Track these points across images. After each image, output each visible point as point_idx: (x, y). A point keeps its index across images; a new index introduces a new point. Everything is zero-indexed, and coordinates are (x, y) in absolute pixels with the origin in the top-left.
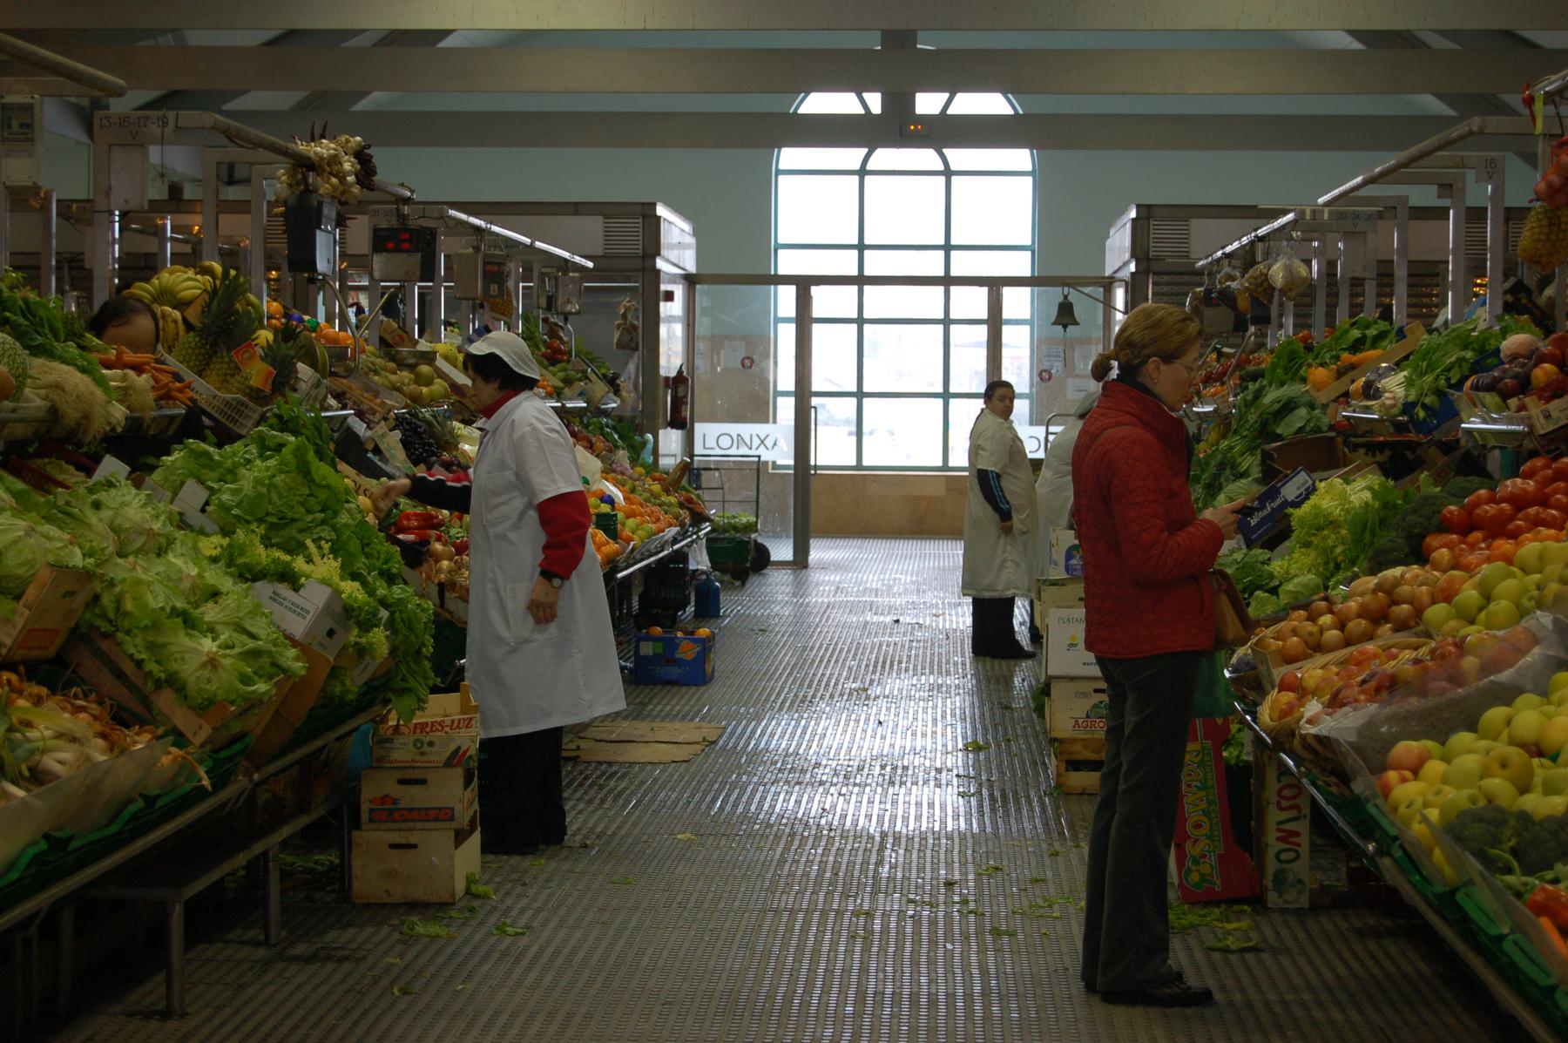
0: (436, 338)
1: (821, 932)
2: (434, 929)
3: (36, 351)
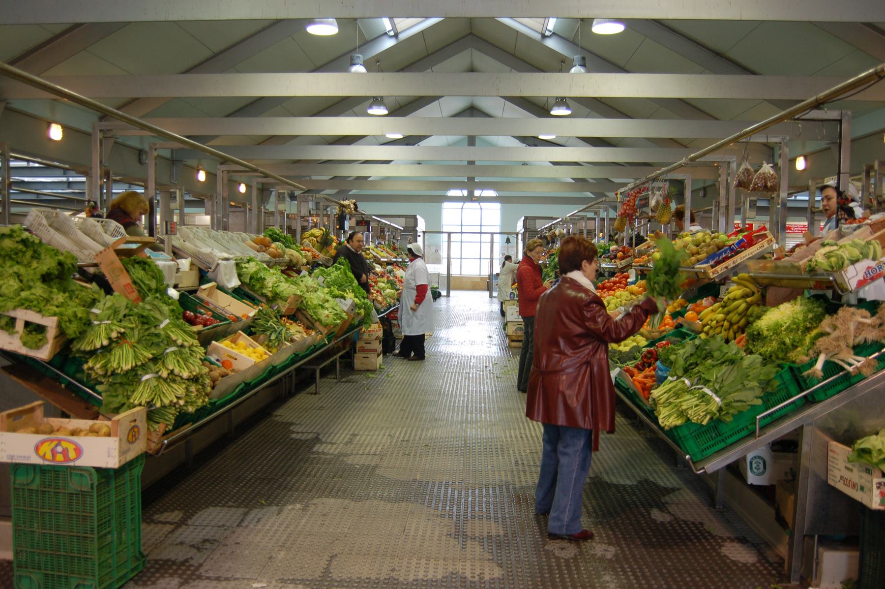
0: (369, 245)
1: (458, 377)
2: (373, 376)
3: (286, 247)
